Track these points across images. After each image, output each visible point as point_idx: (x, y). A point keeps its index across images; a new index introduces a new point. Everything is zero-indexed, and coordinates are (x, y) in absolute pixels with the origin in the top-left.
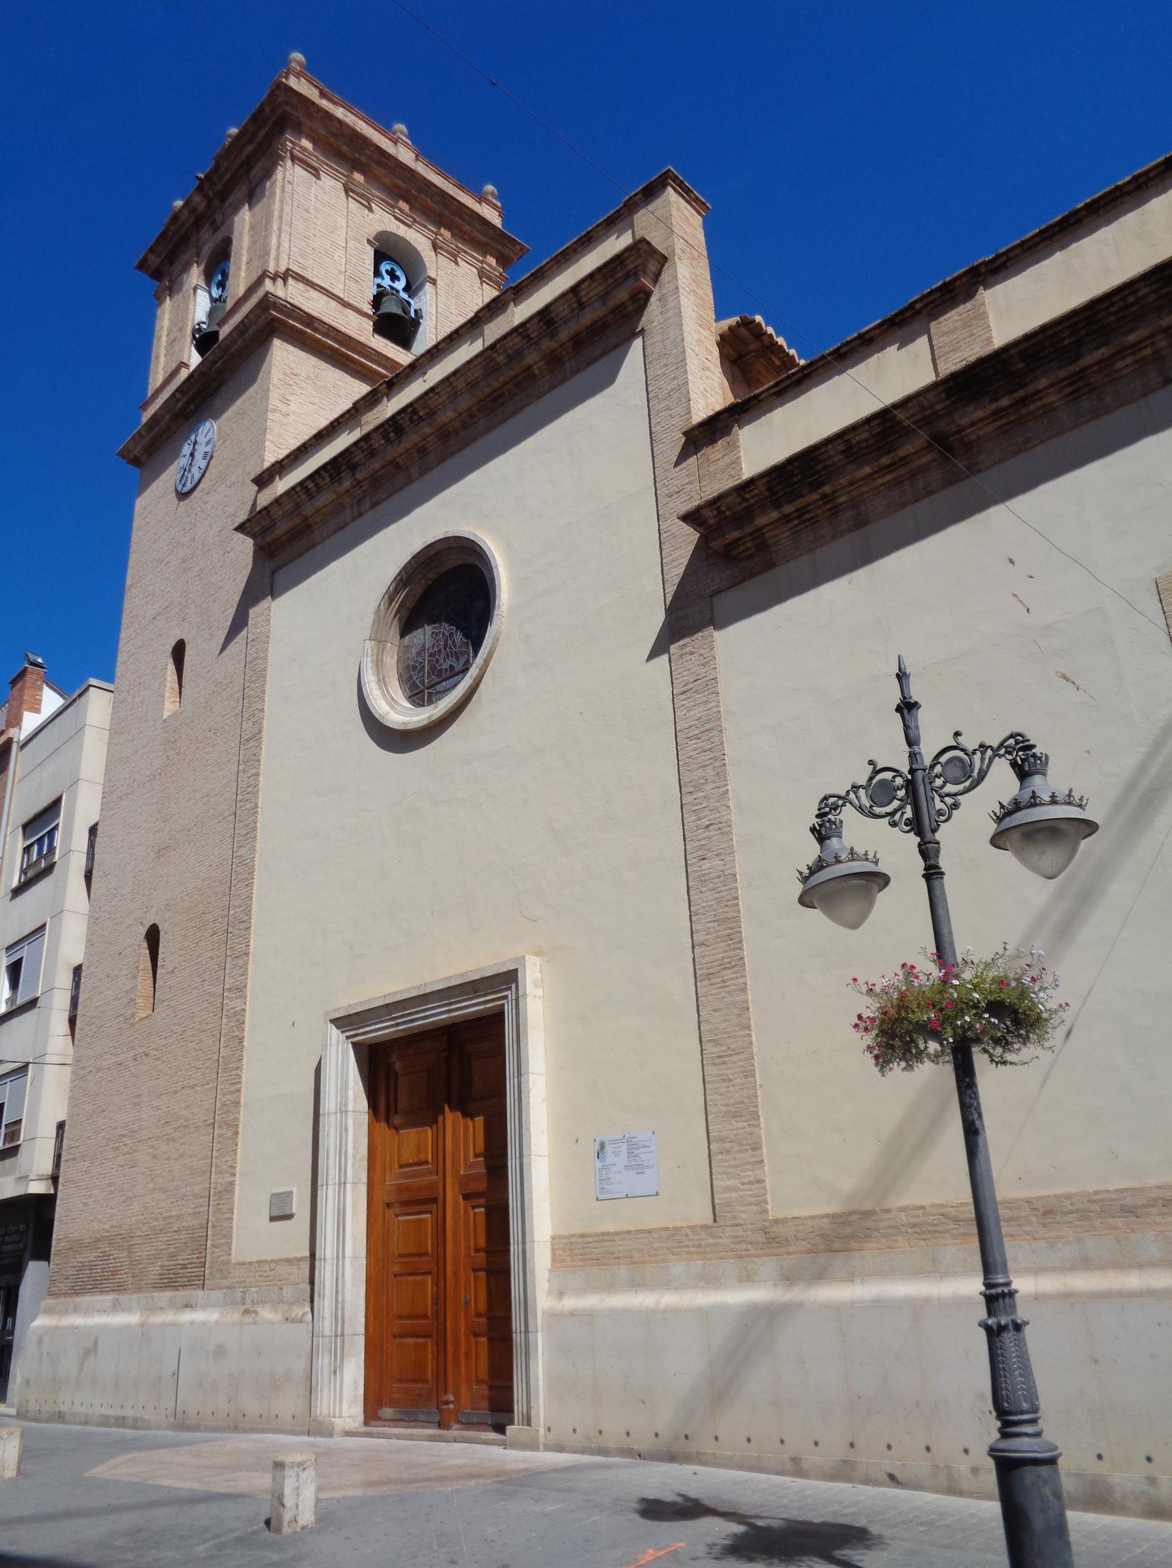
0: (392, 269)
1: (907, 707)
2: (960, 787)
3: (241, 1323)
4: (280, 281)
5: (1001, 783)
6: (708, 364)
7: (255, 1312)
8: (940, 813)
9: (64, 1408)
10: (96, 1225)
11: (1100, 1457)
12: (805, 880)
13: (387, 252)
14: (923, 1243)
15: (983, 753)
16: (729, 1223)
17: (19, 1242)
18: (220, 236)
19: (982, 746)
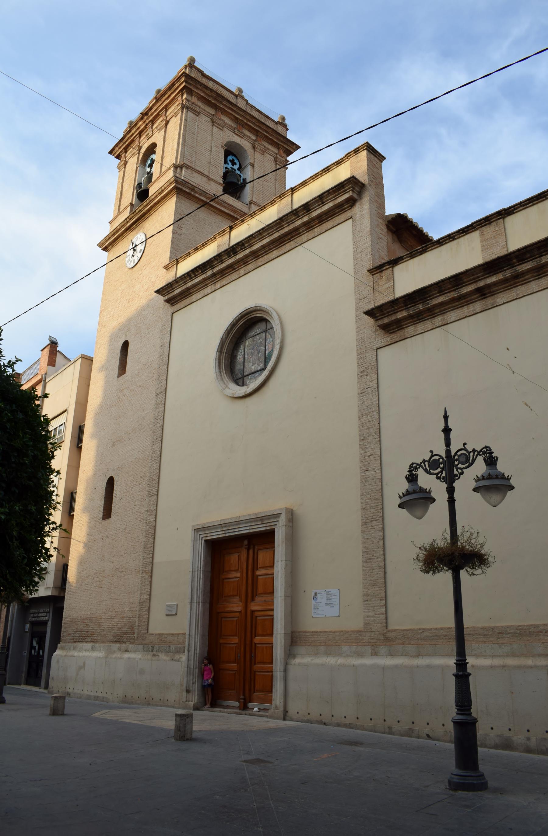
0: (233, 159)
1: (447, 431)
2: (464, 466)
5: (479, 467)
7: (158, 655)
8: (456, 475)
9: (70, 691)
10: (83, 612)
11: (510, 730)
13: (231, 152)
17: (46, 616)
19: (474, 451)
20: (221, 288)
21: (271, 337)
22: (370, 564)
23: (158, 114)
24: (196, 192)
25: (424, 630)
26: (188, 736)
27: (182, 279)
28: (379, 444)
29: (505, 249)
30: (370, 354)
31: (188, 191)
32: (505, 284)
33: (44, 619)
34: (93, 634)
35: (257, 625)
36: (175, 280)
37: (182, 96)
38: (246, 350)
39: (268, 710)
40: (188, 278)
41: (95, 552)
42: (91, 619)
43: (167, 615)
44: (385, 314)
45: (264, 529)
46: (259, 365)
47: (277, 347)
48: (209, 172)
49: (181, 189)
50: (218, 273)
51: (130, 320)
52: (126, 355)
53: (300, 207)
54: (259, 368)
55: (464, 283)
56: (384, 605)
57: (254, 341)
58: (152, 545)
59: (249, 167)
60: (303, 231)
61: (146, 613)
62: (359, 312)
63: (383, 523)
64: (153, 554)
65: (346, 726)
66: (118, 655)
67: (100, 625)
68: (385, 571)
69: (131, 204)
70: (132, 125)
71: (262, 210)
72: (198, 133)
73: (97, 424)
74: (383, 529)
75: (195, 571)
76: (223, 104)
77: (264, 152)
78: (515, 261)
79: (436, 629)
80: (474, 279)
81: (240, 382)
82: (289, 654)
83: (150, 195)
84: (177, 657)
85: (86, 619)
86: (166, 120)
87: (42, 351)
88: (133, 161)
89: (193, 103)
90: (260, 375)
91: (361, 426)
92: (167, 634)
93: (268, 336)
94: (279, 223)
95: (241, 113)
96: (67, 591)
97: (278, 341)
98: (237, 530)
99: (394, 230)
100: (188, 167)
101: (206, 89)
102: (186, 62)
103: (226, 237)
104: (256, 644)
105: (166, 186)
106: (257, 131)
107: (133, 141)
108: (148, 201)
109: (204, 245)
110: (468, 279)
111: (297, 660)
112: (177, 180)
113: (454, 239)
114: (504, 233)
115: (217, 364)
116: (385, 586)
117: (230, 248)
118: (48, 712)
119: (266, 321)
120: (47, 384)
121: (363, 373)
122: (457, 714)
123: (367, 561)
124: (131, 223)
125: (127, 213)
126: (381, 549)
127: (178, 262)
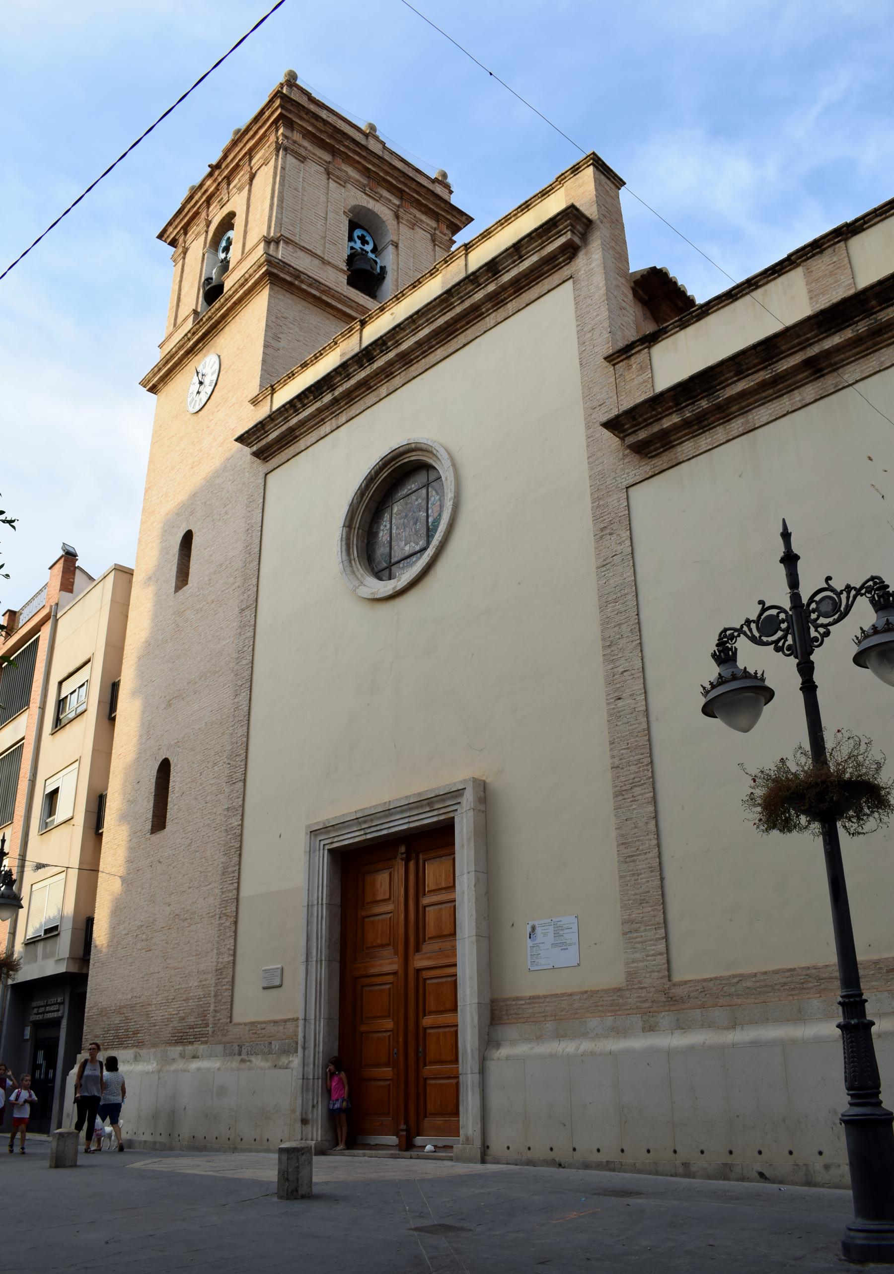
0: (362, 235)
1: (790, 560)
2: (831, 619)
3: (238, 1069)
4: (272, 246)
6: (624, 304)
7: (250, 1061)
8: (816, 639)
10: (120, 996)
12: (706, 692)
13: (360, 222)
14: (791, 998)
15: (848, 593)
16: (636, 987)
17: (58, 1011)
19: (848, 588)
20: (347, 422)
21: (437, 493)
22: (632, 864)
23: (237, 165)
24: (302, 282)
25: (742, 977)
26: (303, 1191)
27: (281, 413)
28: (639, 650)
30: (615, 497)
31: (288, 278)
32: (855, 348)
33: (55, 1015)
34: (136, 1033)
35: (426, 994)
36: (269, 416)
37: (277, 131)
38: (394, 521)
39: (452, 1147)
40: (291, 411)
41: (140, 889)
42: (132, 1007)
43: (264, 988)
44: (639, 424)
45: (435, 819)
46: (417, 544)
48: (324, 252)
49: (278, 276)
50: (342, 398)
51: (194, 495)
52: (189, 556)
53: (481, 268)
54: (418, 548)
55: (782, 352)
56: (663, 938)
57: (406, 504)
58: (237, 868)
59: (391, 249)
60: (488, 310)
61: (227, 987)
63: (654, 788)
64: (238, 883)
65: (600, 1166)
66: (179, 1065)
67: (148, 1015)
68: (661, 874)
69: (195, 312)
71: (415, 287)
72: (304, 189)
73: (141, 674)
75: (312, 905)
76: (344, 146)
77: (415, 224)
78: (874, 303)
79: (765, 973)
80: (800, 344)
82: (489, 1040)
83: (225, 290)
84: (284, 1060)
85: (125, 1007)
86: (251, 172)
87: (50, 568)
88: (197, 245)
89: (295, 142)
91: (605, 622)
92: (265, 1022)
93: (432, 493)
95: (375, 161)
96: (91, 962)
97: (449, 495)
98: (387, 826)
99: (646, 298)
100: (288, 241)
101: (317, 120)
102: (282, 79)
104: (425, 1029)
105: (251, 271)
106: (401, 191)
107: (197, 214)
108: (222, 300)
109: (316, 358)
110: (788, 346)
111: (504, 1051)
112: (270, 261)
113: (758, 287)
114: (848, 265)
115: (344, 547)
116: (663, 903)
117: (361, 351)
118: (48, 1165)
120: (60, 621)
121: (603, 531)
122: (851, 1104)
123: (627, 859)
124: (194, 340)
125: (189, 324)
126: (652, 836)
127: (273, 391)
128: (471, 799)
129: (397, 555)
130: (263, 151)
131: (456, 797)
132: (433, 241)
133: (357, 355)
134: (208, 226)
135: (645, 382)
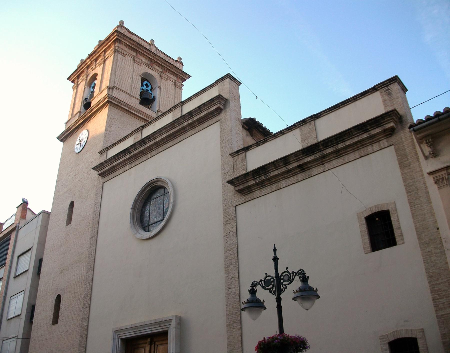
1: (275, 259)
2: (287, 283)
4: (111, 90)
5: (297, 283)
13: (146, 79)
18: (94, 72)
19: (293, 272)
23: (99, 55)
24: (122, 104)
29: (316, 140)
31: (116, 103)
36: (105, 161)
45: (161, 330)
47: (171, 205)
52: (72, 211)
54: (159, 220)
57: (156, 201)
59: (158, 89)
62: (224, 182)
70: (83, 62)
74: (241, 329)
81: (147, 228)
83: (92, 105)
88: (82, 85)
90: (160, 224)
91: (226, 258)
93: (166, 198)
94: (173, 124)
97: (172, 201)
99: (248, 128)
100: (117, 88)
103: (139, 134)
106: (163, 66)
107: (83, 72)
113: (284, 134)
119: (164, 188)
121: (227, 222)
125: (77, 118)
126: (240, 343)
128: (174, 323)
129: (152, 221)
130: (109, 51)
131: (169, 322)
132: (175, 85)
133: (139, 141)
134: (87, 77)
135: (243, 165)
